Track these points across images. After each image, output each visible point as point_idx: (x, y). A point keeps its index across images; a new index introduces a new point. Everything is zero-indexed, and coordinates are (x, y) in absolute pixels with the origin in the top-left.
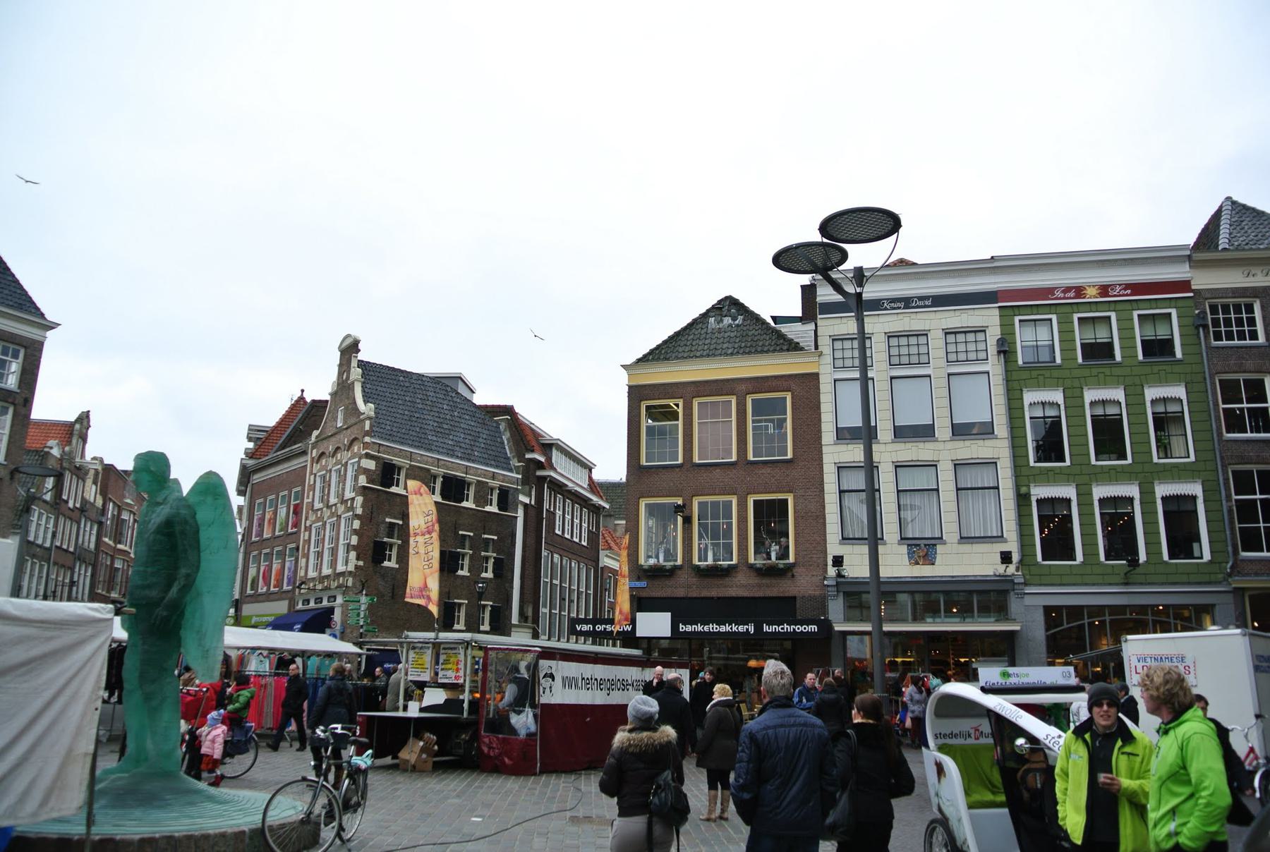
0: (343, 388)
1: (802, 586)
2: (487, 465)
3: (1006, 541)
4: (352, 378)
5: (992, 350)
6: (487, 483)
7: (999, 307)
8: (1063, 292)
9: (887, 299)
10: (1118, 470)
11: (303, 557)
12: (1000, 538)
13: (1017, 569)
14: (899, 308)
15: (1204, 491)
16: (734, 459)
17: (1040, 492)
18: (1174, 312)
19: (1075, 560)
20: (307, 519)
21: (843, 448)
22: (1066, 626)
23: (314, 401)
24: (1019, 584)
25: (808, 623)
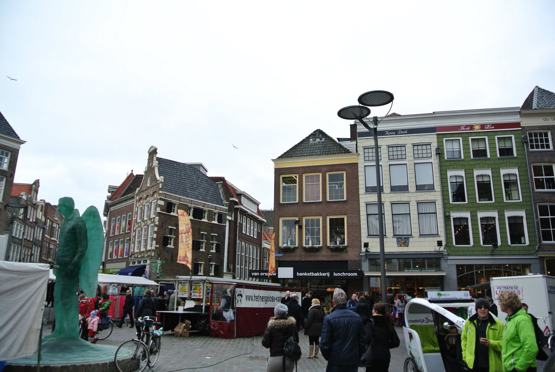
0: (150, 170)
2: (213, 203)
3: (440, 236)
4: (154, 165)
5: (434, 153)
6: (213, 211)
7: (437, 134)
8: (464, 127)
9: (388, 131)
10: (489, 205)
11: (132, 243)
12: (437, 235)
13: (445, 249)
14: (393, 134)
15: (526, 214)
16: (321, 200)
17: (454, 215)
18: (513, 136)
19: (470, 244)
20: (134, 226)
21: (368, 195)
22: (466, 273)
23: (137, 175)
24: (445, 255)
25: (353, 272)
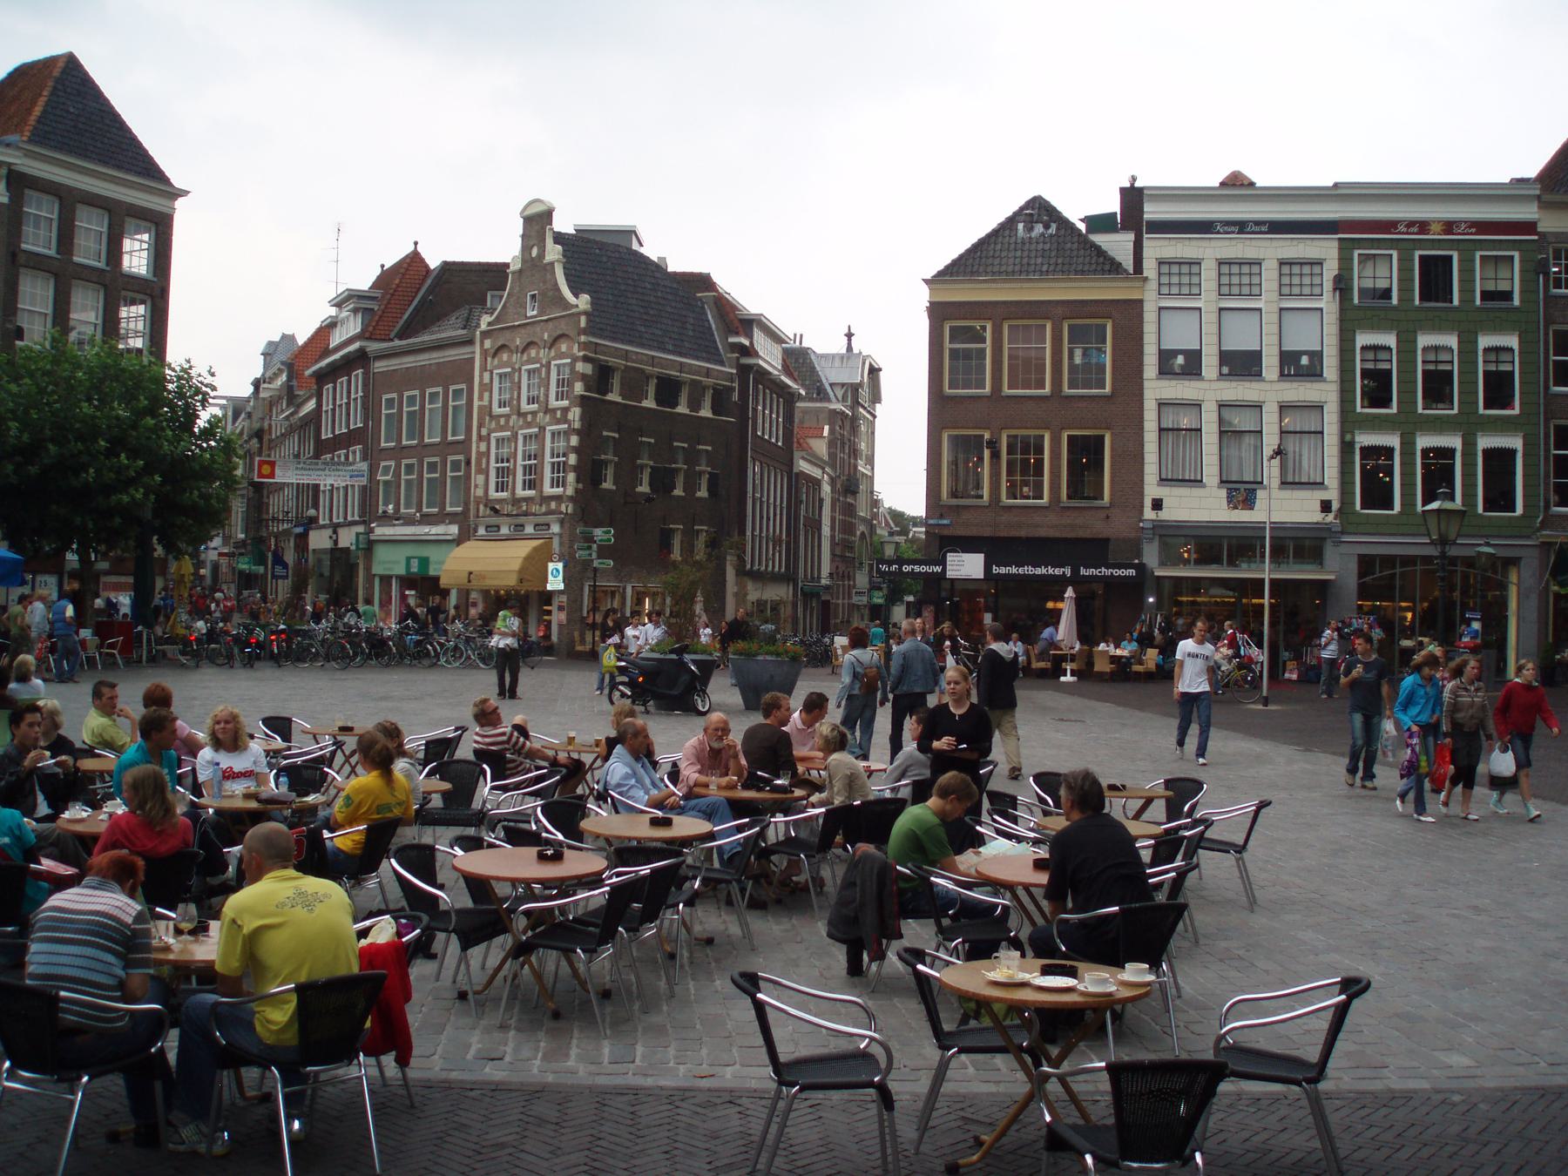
0: (533, 264)
1: (1116, 528)
2: (697, 358)
3: (1326, 488)
4: (549, 258)
5: (1328, 285)
6: (701, 381)
7: (1339, 239)
8: (1405, 226)
9: (1221, 222)
11: (479, 471)
12: (1320, 485)
13: (1335, 519)
14: (1233, 233)
17: (1365, 439)
18: (1516, 255)
20: (480, 426)
21: (1286, 385)
22: (1378, 575)
23: (447, 267)
24: (1336, 532)
25: (1127, 567)
